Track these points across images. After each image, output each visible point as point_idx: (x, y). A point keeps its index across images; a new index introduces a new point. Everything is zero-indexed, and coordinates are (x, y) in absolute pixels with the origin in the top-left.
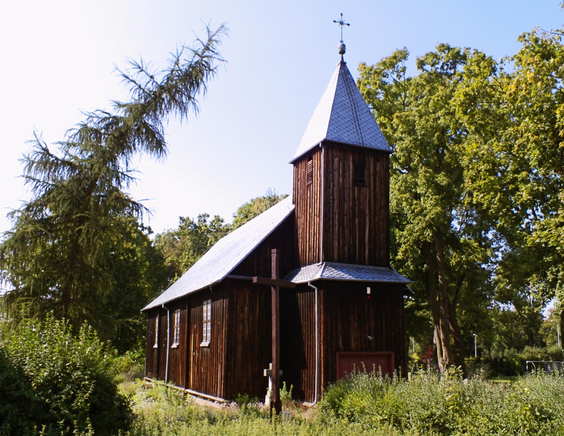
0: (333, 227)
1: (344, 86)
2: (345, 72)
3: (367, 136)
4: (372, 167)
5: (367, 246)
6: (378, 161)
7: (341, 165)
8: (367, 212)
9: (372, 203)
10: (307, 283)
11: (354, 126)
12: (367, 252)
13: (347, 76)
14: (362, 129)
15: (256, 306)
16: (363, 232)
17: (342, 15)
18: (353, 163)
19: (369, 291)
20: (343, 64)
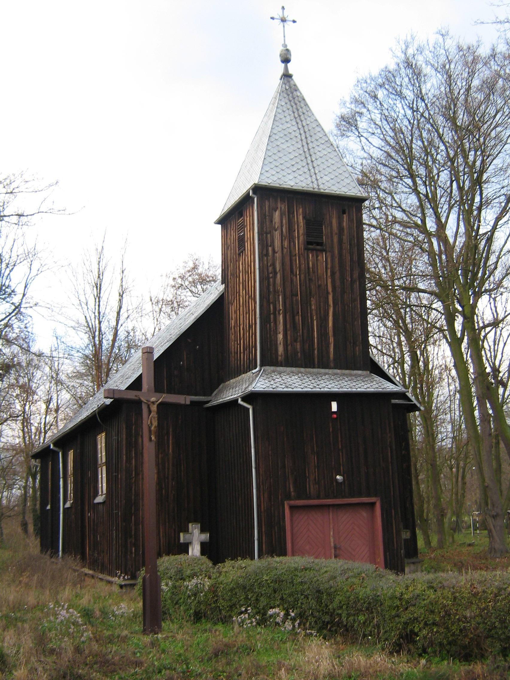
0: (274, 314)
1: (289, 107)
2: (290, 87)
3: (325, 177)
4: (334, 221)
5: (332, 340)
6: (344, 212)
7: (284, 221)
8: (330, 289)
9: (337, 275)
10: (236, 401)
11: (305, 164)
12: (332, 350)
13: (295, 93)
14: (317, 168)
15: (168, 440)
16: (323, 320)
17: (283, 8)
18: (304, 218)
19: (334, 406)
20: (287, 76)
